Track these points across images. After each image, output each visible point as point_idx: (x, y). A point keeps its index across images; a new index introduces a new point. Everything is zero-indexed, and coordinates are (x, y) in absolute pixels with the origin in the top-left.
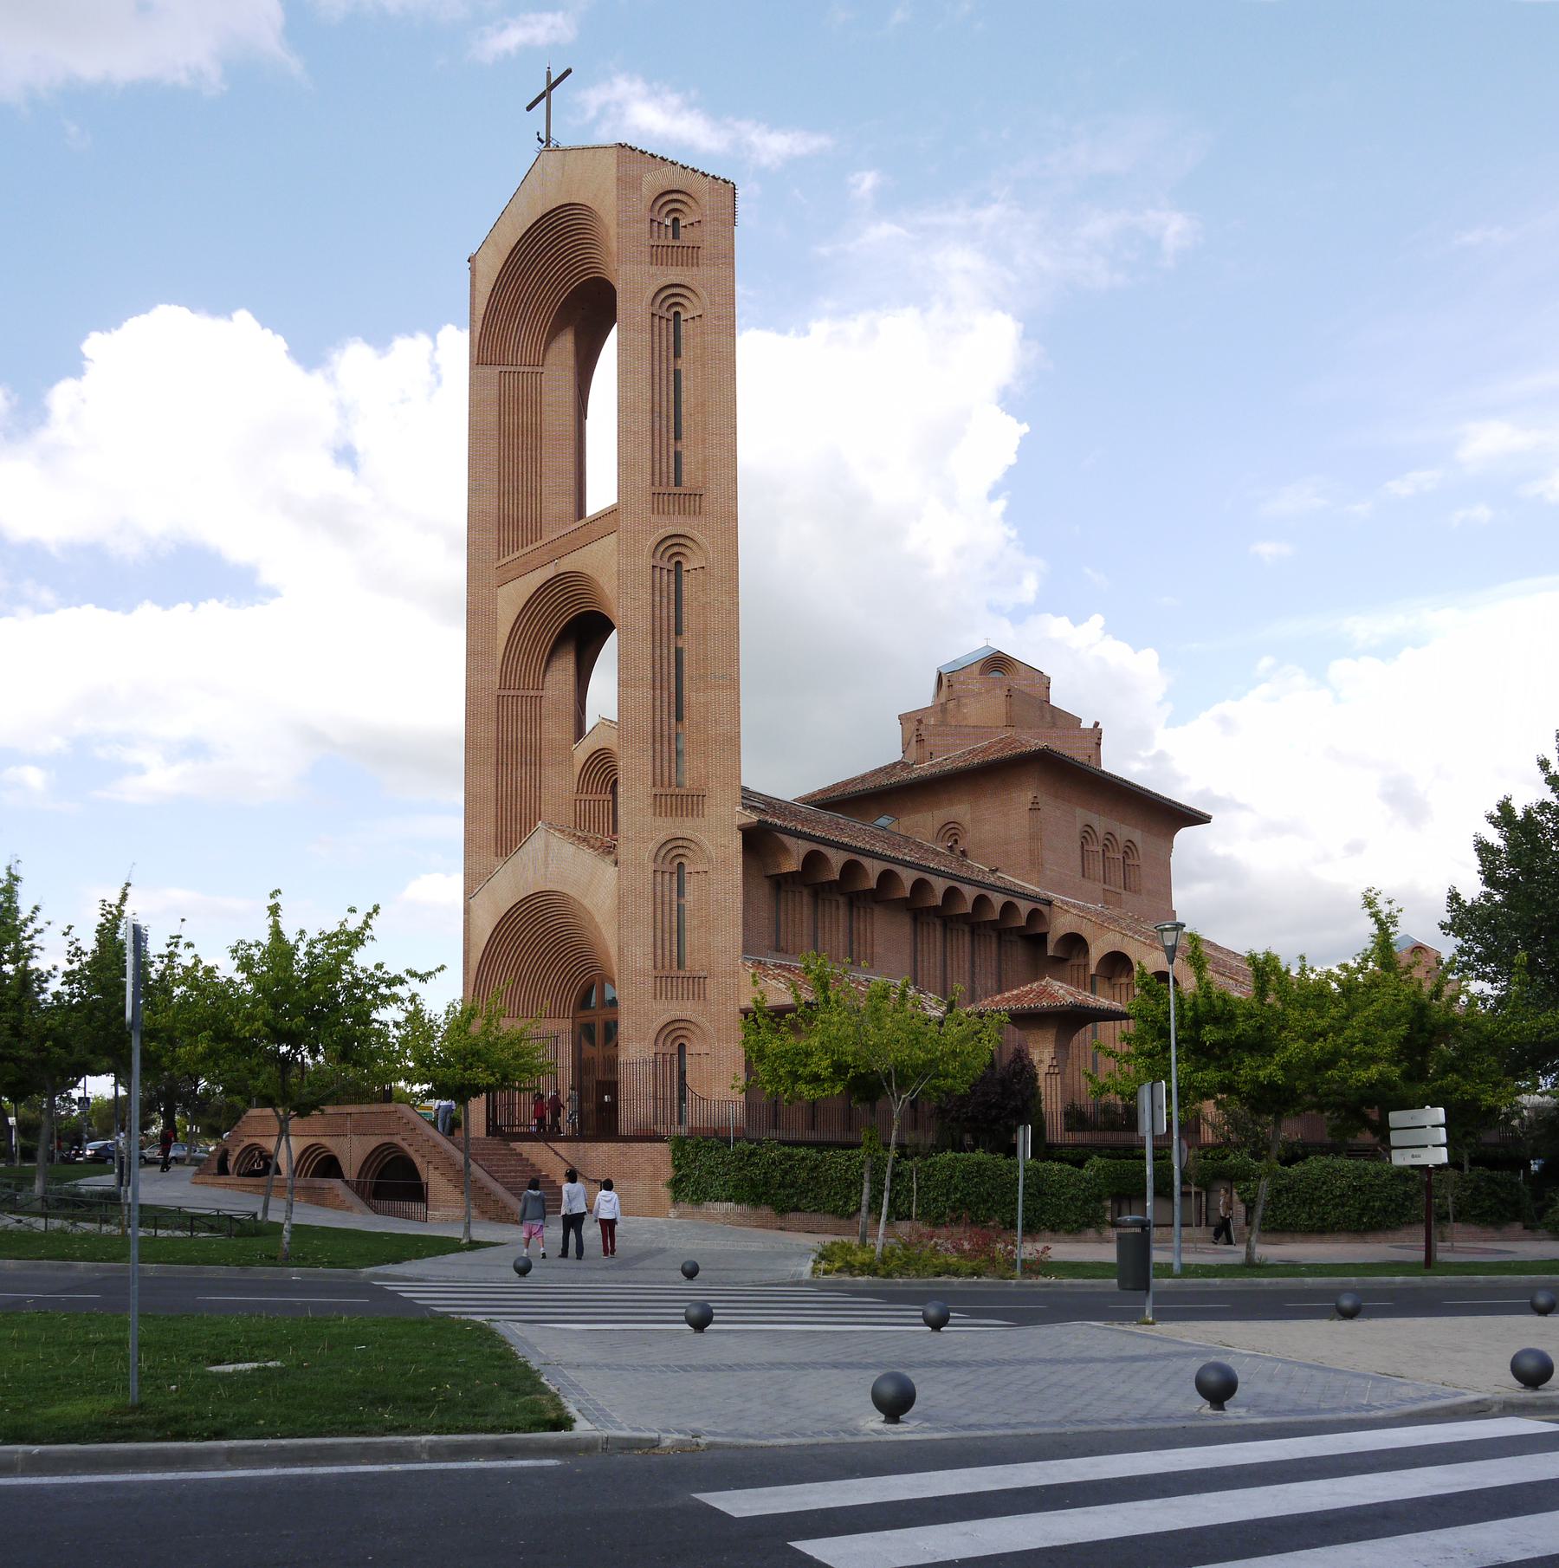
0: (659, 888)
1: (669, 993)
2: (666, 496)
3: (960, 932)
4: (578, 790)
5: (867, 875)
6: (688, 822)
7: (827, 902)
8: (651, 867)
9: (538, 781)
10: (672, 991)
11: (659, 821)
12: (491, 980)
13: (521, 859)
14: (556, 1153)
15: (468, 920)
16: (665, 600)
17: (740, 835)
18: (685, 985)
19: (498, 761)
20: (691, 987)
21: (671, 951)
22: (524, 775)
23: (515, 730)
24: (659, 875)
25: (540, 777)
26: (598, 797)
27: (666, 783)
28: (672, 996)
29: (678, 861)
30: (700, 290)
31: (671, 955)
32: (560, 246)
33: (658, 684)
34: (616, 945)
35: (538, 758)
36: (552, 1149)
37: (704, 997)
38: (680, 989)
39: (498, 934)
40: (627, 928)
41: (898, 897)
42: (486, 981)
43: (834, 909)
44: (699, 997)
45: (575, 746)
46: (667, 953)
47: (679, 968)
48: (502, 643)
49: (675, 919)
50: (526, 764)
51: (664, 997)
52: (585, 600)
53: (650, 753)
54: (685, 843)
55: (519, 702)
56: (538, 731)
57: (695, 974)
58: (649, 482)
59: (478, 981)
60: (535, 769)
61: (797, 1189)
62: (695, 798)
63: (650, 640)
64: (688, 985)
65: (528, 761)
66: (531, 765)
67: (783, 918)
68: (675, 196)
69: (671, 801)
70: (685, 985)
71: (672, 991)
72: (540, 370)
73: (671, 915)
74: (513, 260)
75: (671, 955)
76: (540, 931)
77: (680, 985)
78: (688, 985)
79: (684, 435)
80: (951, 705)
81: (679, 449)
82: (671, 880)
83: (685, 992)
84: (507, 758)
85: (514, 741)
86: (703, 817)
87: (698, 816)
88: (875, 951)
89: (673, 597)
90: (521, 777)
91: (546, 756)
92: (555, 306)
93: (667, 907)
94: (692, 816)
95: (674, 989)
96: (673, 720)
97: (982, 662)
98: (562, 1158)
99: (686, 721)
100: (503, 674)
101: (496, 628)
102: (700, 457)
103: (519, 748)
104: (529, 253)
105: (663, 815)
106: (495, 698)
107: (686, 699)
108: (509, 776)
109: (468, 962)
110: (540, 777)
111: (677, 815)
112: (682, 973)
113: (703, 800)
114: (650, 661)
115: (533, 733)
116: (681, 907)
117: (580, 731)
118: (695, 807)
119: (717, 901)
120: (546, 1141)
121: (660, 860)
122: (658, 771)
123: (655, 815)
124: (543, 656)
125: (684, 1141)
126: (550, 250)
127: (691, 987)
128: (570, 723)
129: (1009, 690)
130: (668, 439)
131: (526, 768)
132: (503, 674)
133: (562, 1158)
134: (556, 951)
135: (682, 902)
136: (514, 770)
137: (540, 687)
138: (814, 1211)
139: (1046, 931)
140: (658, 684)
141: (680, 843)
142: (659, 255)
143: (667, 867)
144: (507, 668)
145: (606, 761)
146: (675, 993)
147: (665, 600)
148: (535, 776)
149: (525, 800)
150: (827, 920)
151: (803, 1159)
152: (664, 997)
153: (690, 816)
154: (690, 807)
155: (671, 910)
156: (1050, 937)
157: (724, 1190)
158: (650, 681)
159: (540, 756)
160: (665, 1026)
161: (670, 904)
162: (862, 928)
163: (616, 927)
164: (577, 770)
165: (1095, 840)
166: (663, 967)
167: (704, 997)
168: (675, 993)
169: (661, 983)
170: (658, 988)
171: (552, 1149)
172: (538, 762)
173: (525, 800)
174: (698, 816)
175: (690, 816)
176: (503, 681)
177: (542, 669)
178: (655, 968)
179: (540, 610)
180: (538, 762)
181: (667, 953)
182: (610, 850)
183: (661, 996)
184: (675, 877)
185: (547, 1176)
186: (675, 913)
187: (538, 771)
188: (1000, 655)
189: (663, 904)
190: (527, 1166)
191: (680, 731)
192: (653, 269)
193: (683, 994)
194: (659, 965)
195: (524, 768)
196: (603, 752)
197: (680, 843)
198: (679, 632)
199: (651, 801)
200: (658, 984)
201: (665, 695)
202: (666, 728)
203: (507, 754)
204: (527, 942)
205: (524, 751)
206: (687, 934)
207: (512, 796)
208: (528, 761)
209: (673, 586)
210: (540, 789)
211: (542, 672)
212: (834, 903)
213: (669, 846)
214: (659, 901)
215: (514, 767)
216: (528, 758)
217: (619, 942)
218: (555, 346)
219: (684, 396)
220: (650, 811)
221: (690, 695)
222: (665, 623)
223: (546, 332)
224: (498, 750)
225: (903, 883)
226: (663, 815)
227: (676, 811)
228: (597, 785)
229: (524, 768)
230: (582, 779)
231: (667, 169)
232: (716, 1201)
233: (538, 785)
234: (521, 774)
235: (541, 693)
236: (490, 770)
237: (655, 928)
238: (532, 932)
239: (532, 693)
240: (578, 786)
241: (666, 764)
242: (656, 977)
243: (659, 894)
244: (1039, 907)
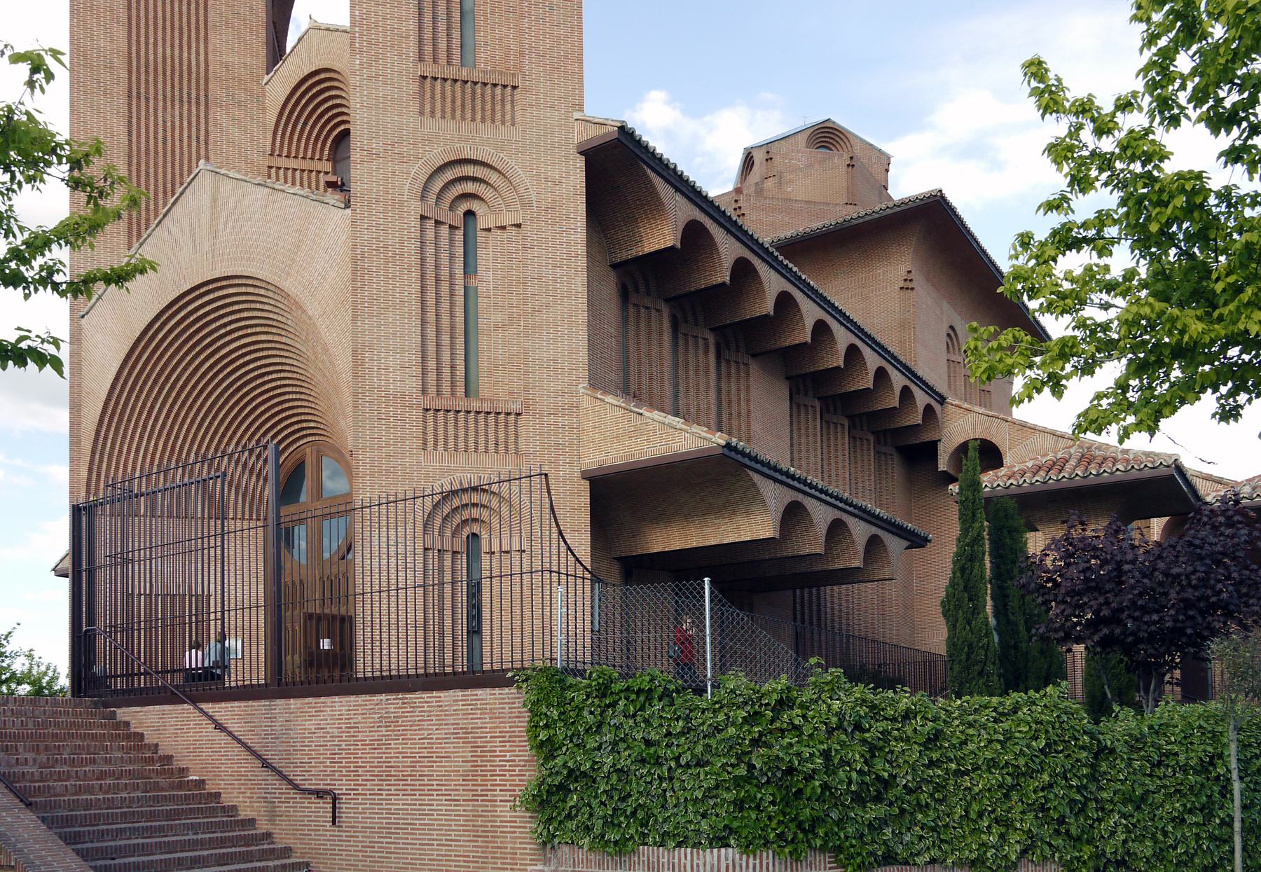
0: (430, 250)
3: (832, 426)
4: (273, 150)
5: (761, 290)
6: (486, 131)
8: (415, 208)
10: (456, 437)
12: (120, 452)
13: (170, 233)
14: (219, 727)
15: (79, 354)
17: (581, 163)
19: (130, 91)
21: (453, 367)
26: (307, 165)
31: (453, 375)
34: (349, 352)
35: (202, 93)
36: (211, 718)
37: (517, 448)
39: (130, 374)
41: (793, 343)
43: (701, 351)
45: (267, 78)
46: (446, 370)
47: (467, 394)
50: (181, 101)
52: (287, 397)
54: (479, 172)
56: (202, 46)
57: (501, 407)
59: (97, 456)
61: (891, 804)
64: (486, 425)
65: (185, 96)
67: (632, 348)
69: (453, 92)
71: (456, 437)
73: (452, 304)
75: (453, 375)
76: (207, 365)
78: (486, 425)
80: (770, 183)
82: (452, 241)
85: (160, 60)
86: (513, 125)
87: (503, 123)
88: (752, 428)
90: (173, 123)
91: (216, 90)
93: (445, 287)
94: (493, 121)
95: (461, 434)
98: (234, 738)
105: (438, 115)
108: (152, 118)
111: (463, 118)
112: (475, 405)
113: (512, 95)
115: (194, 49)
116: (471, 294)
117: (276, 51)
118: (498, 107)
120: (194, 700)
121: (432, 198)
122: (428, 36)
125: (561, 681)
128: (259, 40)
129: (851, 158)
133: (234, 738)
135: (473, 282)
138: (933, 861)
139: (937, 438)
141: (469, 170)
143: (443, 214)
145: (323, 86)
149: (181, 160)
151: (907, 715)
153: (488, 122)
154: (488, 107)
155: (452, 295)
156: (941, 447)
157: (704, 816)
161: (452, 284)
162: (734, 391)
163: (348, 318)
165: (956, 348)
166: (439, 393)
167: (517, 448)
169: (435, 421)
171: (211, 718)
172: (202, 99)
173: (181, 160)
175: (488, 122)
180: (202, 99)
181: (446, 370)
183: (436, 445)
185: (201, 783)
186: (460, 301)
187: (202, 115)
188: (831, 125)
189: (437, 280)
190: (150, 761)
195: (177, 107)
196: (323, 76)
197: (469, 170)
199: (414, 86)
203: (147, 81)
205: (177, 80)
206: (483, 338)
207: (156, 152)
208: (185, 96)
212: (701, 342)
213: (450, 175)
214: (430, 272)
215: (160, 104)
216: (185, 91)
217: (355, 341)
220: (414, 105)
224: (130, 72)
226: (438, 115)
229: (177, 107)
230: (280, 132)
232: (679, 845)
233: (202, 138)
234: (173, 116)
236: (118, 103)
237: (423, 322)
238: (191, 369)
242: (427, 410)
243: (430, 260)
244: (934, 403)
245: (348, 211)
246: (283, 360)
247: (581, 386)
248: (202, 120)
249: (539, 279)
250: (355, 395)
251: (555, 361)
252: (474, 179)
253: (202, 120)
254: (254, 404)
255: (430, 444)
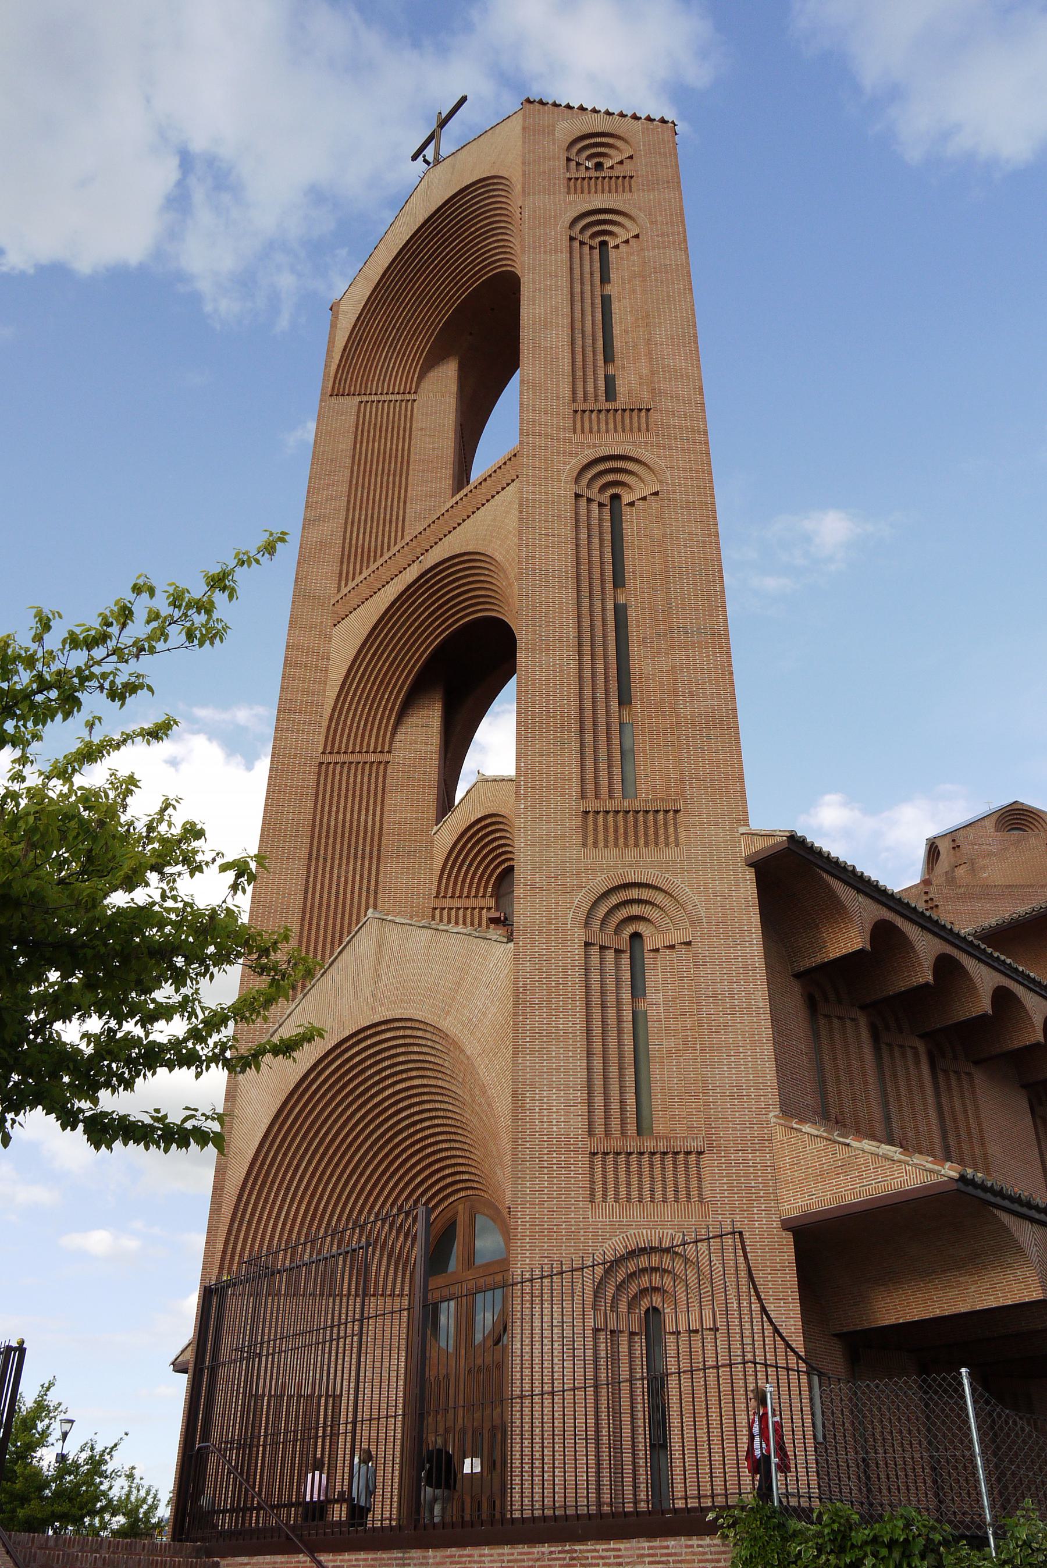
0: (595, 976)
1: (623, 1190)
2: (595, 413)
4: (438, 893)
6: (649, 855)
7: (896, 1049)
8: (579, 936)
9: (373, 883)
10: (628, 1184)
11: (594, 855)
13: (333, 981)
16: (596, 540)
17: (750, 875)
18: (657, 1171)
20: (669, 1174)
21: (622, 1102)
22: (350, 874)
23: (341, 810)
24: (595, 951)
25: (377, 875)
27: (604, 790)
28: (628, 1194)
29: (630, 929)
30: (633, 212)
31: (623, 1110)
32: (408, 1165)
33: (587, 647)
34: (508, 1092)
37: (700, 1195)
38: (646, 1179)
40: (532, 1052)
42: (250, 1222)
44: (688, 1194)
45: (435, 828)
46: (615, 1106)
47: (639, 1132)
48: (332, 693)
49: (628, 1039)
51: (610, 1198)
53: (575, 746)
54: (644, 894)
55: (353, 771)
56: (378, 809)
57: (679, 1145)
58: (567, 395)
60: (370, 864)
62: (661, 816)
63: (571, 585)
64: (663, 1168)
66: (363, 858)
67: (828, 1065)
68: (634, 893)
70: (657, 1171)
71: (628, 1184)
72: (413, 397)
74: (386, 283)
75: (623, 1110)
76: (358, 1116)
77: (646, 1170)
78: (663, 1168)
79: (618, 356)
81: (606, 292)
83: (658, 1186)
84: (326, 850)
86: (677, 846)
88: (990, 1151)
89: (608, 537)
92: (421, 656)
93: (612, 1013)
95: (634, 1180)
96: (614, 704)
97: (1000, 813)
99: (637, 704)
100: (331, 733)
101: (326, 677)
102: (645, 372)
103: (347, 835)
104: (406, 271)
105: (601, 844)
106: (315, 768)
107: (635, 671)
108: (327, 876)
109: (222, 1189)
110: (377, 875)
111: (626, 845)
112: (649, 1145)
113: (675, 819)
114: (573, 615)
116: (640, 1018)
117: (446, 804)
118: (661, 831)
119: (715, 996)
121: (596, 924)
122: (590, 775)
123: (585, 845)
124: (394, 704)
126: (433, 262)
127: (669, 1174)
128: (430, 797)
130: (595, 361)
131: (355, 863)
132: (331, 733)
134: (386, 1156)
135: (642, 1006)
136: (336, 867)
137: (386, 749)
140: (587, 647)
141: (634, 893)
142: (573, 184)
144: (337, 724)
146: (635, 1186)
147: (596, 540)
148: (370, 874)
150: (902, 1083)
152: (610, 1198)
155: (620, 1021)
158: (573, 642)
159: (379, 846)
160: (605, 895)
161: (619, 1010)
163: (509, 1055)
164: (438, 862)
166: (607, 1133)
167: (700, 1195)
168: (635, 1186)
170: (598, 1176)
172: (375, 853)
174: (667, 845)
176: (329, 744)
177: (392, 721)
178: (591, 1132)
179: (392, 638)
180: (375, 853)
181: (615, 1106)
182: (503, 922)
184: (625, 959)
186: (628, 1027)
189: (604, 1006)
191: (626, 719)
192: (572, 197)
193: (652, 1190)
194: (600, 1129)
195: (352, 863)
198: (619, 581)
199: (577, 822)
200: (598, 1170)
201: (600, 665)
202: (601, 711)
204: (332, 1141)
206: (655, 1068)
209: (607, 526)
210: (376, 893)
211: (390, 728)
213: (614, 900)
214: (596, 999)
215: (337, 862)
216: (360, 848)
217: (515, 1081)
218: (433, 375)
219: (616, 318)
220: (577, 838)
221: (641, 662)
222: (596, 568)
223: (417, 373)
225: (1030, 1018)
226: (601, 844)
227: (626, 838)
228: (471, 884)
229: (352, 863)
231: (588, 117)
233: (372, 888)
235: (386, 757)
237: (589, 1054)
239: (372, 758)
240: (439, 887)
241: (603, 766)
242: (594, 1154)
243: (595, 986)
245: (511, 945)
246: (438, 1105)
247: (771, 1114)
248: (374, 873)
249: (715, 996)
250: (515, 1140)
251: (739, 1087)
252: (640, 901)
253: (374, 873)
254: (412, 1110)
255: (599, 1195)
